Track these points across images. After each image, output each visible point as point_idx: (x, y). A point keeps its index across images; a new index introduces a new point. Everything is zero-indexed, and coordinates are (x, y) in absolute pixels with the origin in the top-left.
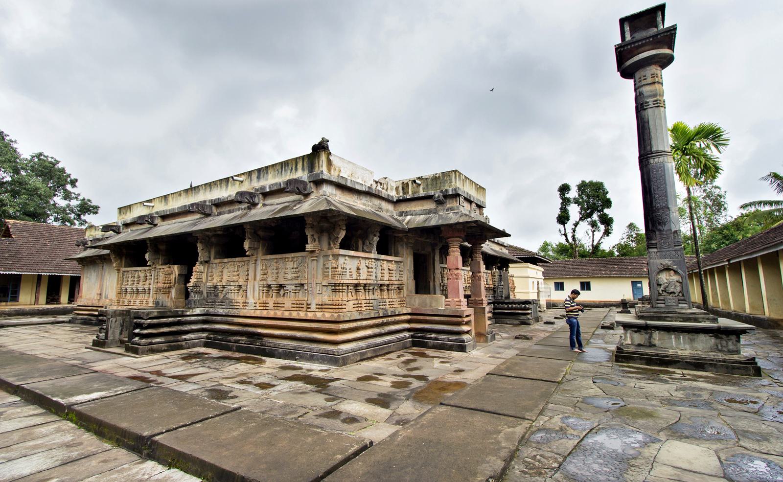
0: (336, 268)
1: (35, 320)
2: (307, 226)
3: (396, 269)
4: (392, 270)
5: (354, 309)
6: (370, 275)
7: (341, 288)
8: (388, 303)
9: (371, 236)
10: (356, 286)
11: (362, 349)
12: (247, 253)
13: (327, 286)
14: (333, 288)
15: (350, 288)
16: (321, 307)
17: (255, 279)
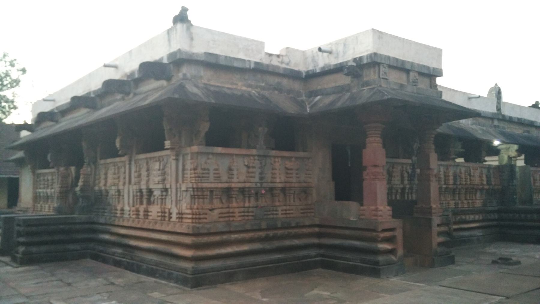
1: (347, 232)
4: (291, 169)
5: (221, 220)
6: (251, 177)
8: (238, 214)
10: (228, 191)
11: (229, 268)
12: (120, 153)
15: (214, 193)
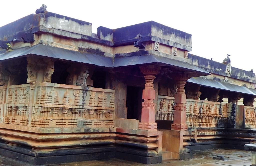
0: (43, 96)
2: (28, 65)
3: (107, 99)
4: (102, 99)
7: (45, 110)
9: (82, 73)
10: (62, 109)
13: (38, 108)
14: (41, 110)
16: (34, 123)
17: (5, 102)
